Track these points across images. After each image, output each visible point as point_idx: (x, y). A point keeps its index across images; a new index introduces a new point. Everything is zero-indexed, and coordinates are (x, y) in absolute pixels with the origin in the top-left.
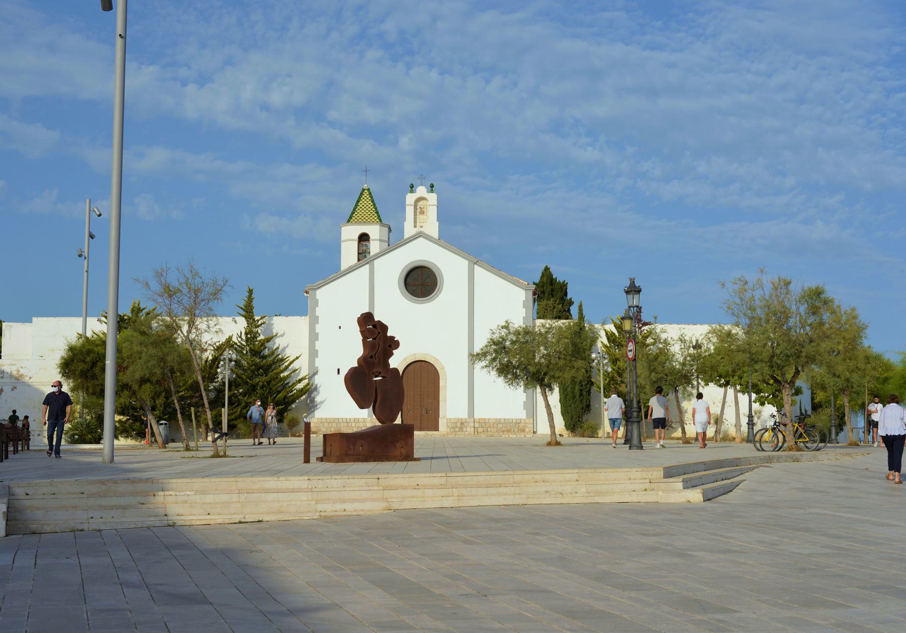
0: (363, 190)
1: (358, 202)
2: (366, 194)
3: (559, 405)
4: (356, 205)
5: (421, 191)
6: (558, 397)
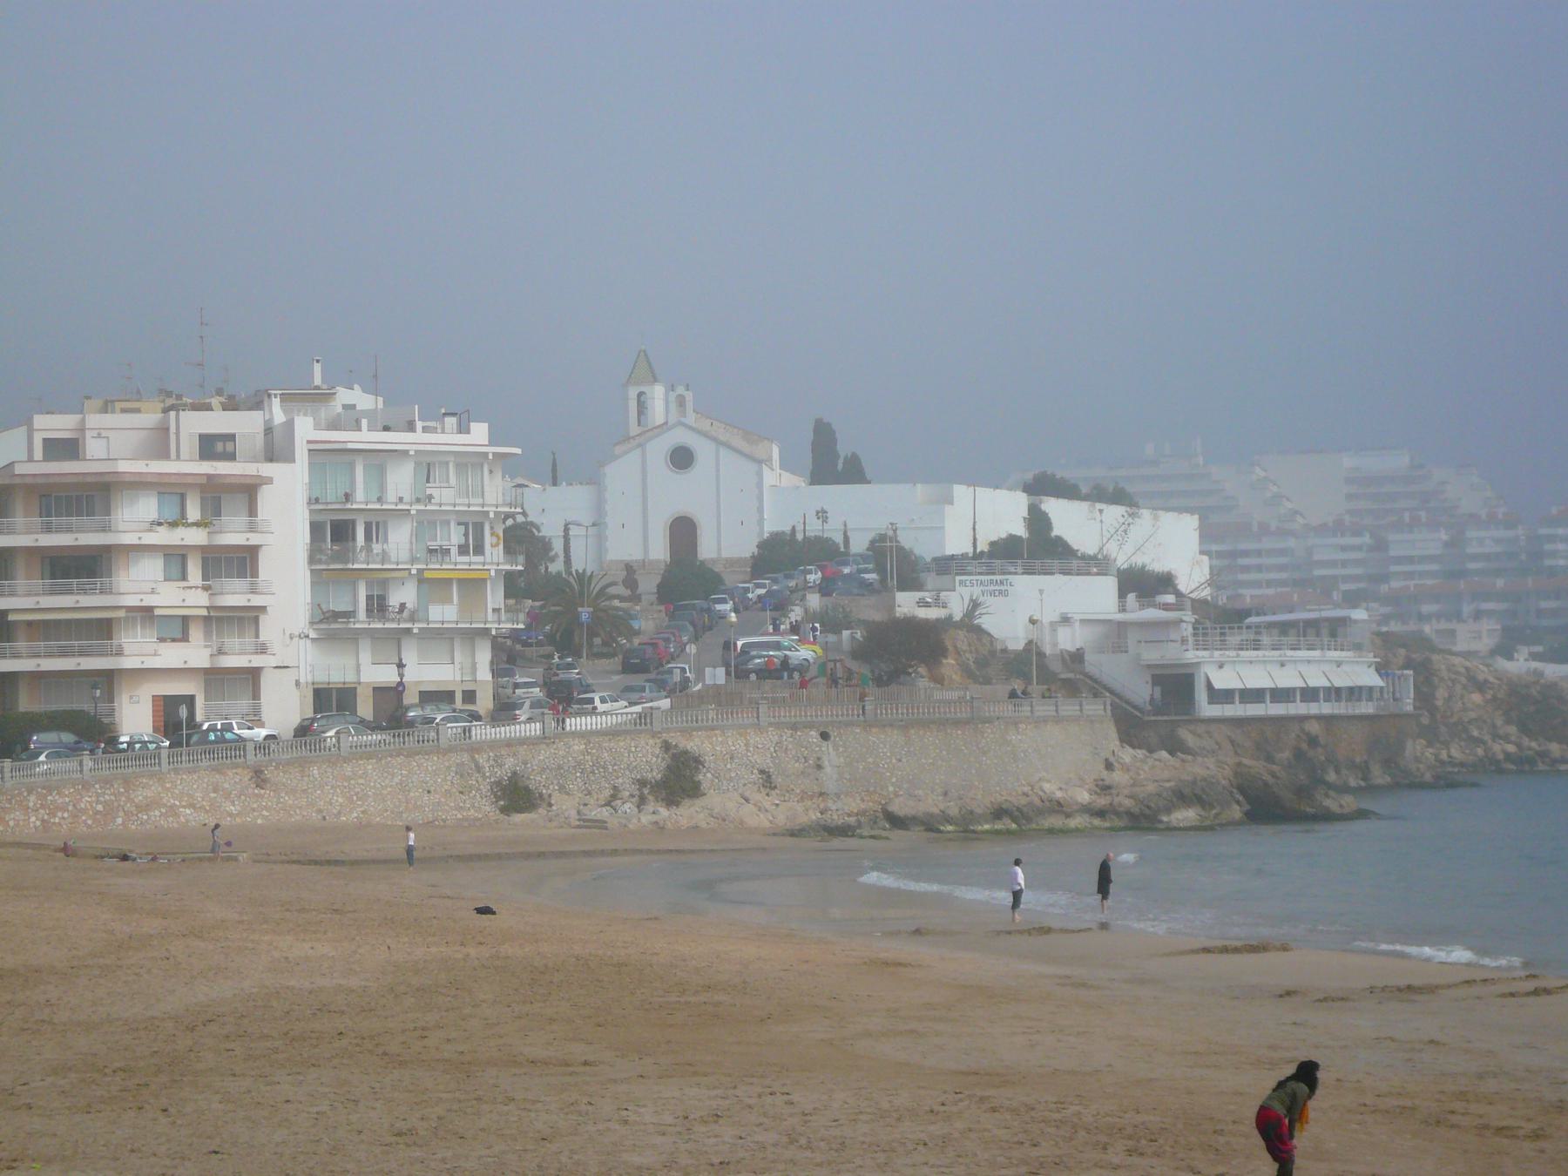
5: (680, 390)
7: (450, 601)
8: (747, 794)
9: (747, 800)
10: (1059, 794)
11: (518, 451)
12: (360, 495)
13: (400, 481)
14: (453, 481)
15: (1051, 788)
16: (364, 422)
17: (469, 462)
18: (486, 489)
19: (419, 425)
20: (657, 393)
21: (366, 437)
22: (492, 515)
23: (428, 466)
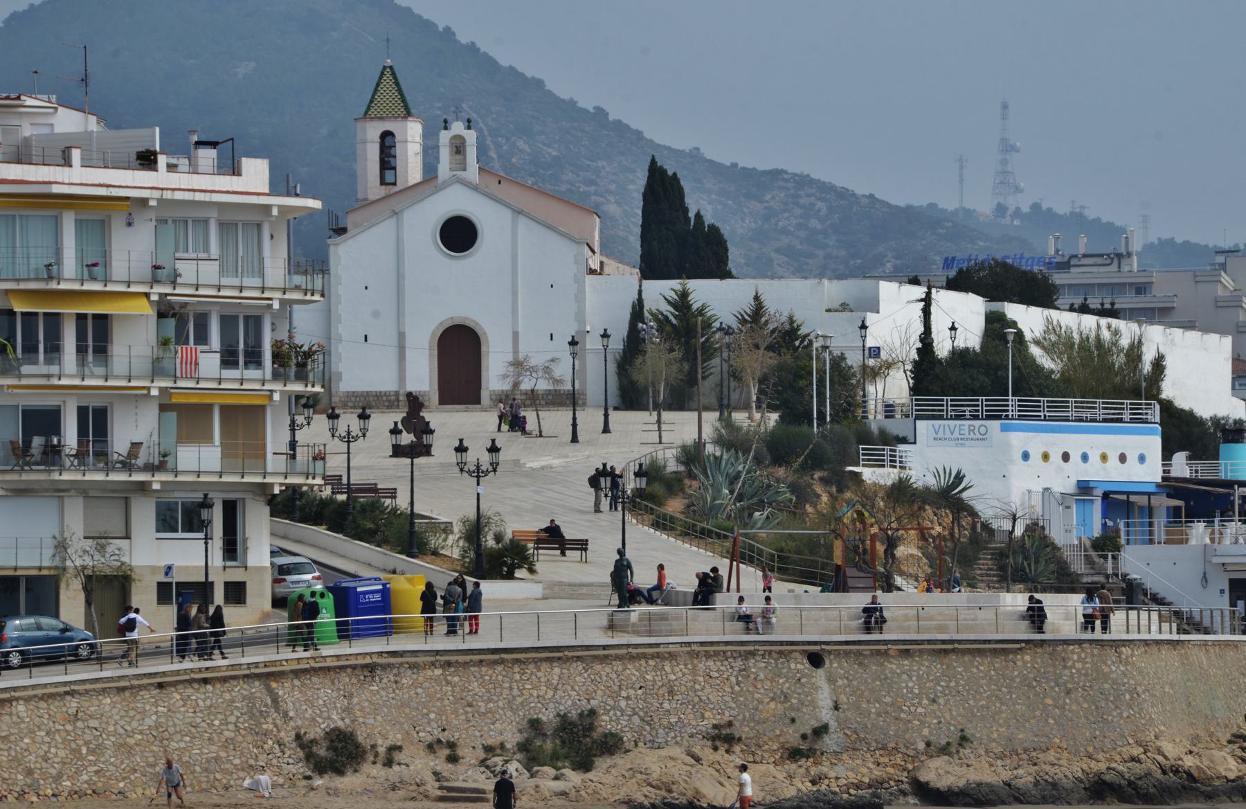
0: (385, 68)
1: (378, 85)
2: (388, 74)
3: (419, 159)
4: (376, 90)
5: (458, 128)
6: (1022, 307)
7: (209, 439)
8: (697, 750)
9: (698, 760)
10: (1189, 762)
11: (316, 204)
12: (70, 265)
13: (132, 250)
14: (214, 250)
15: (1173, 749)
16: (76, 155)
17: (240, 223)
18: (268, 263)
19: (162, 160)
20: (411, 134)
21: (76, 178)
22: (276, 305)
23: (179, 219)
